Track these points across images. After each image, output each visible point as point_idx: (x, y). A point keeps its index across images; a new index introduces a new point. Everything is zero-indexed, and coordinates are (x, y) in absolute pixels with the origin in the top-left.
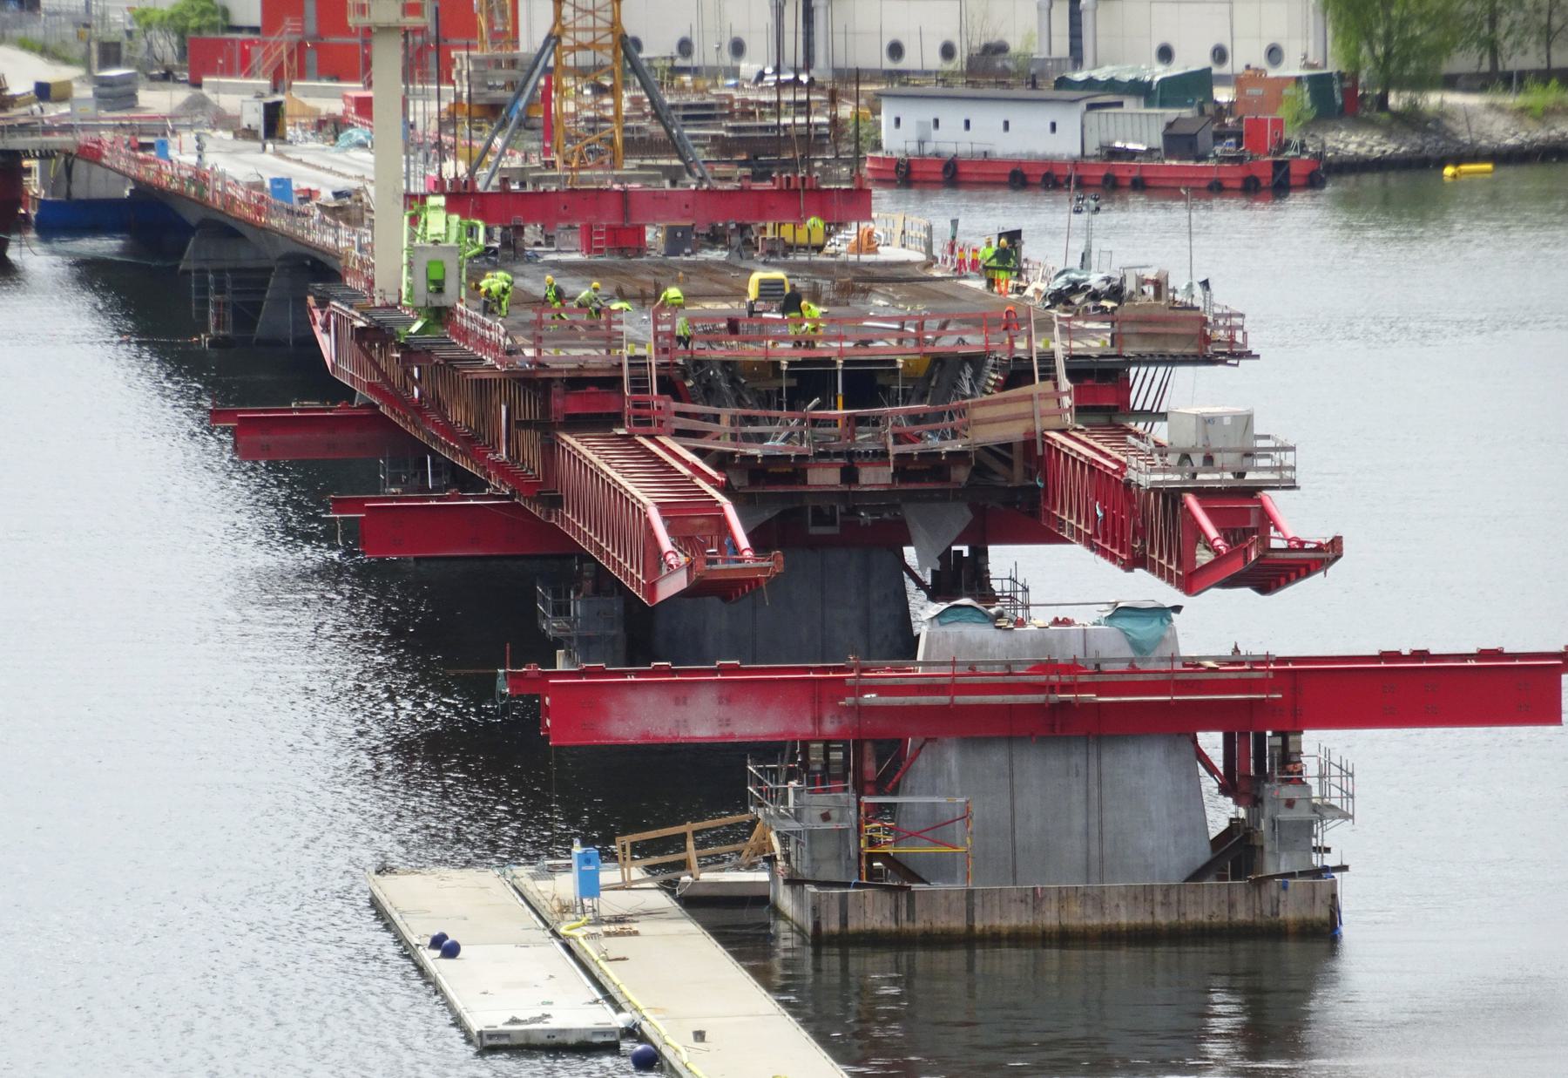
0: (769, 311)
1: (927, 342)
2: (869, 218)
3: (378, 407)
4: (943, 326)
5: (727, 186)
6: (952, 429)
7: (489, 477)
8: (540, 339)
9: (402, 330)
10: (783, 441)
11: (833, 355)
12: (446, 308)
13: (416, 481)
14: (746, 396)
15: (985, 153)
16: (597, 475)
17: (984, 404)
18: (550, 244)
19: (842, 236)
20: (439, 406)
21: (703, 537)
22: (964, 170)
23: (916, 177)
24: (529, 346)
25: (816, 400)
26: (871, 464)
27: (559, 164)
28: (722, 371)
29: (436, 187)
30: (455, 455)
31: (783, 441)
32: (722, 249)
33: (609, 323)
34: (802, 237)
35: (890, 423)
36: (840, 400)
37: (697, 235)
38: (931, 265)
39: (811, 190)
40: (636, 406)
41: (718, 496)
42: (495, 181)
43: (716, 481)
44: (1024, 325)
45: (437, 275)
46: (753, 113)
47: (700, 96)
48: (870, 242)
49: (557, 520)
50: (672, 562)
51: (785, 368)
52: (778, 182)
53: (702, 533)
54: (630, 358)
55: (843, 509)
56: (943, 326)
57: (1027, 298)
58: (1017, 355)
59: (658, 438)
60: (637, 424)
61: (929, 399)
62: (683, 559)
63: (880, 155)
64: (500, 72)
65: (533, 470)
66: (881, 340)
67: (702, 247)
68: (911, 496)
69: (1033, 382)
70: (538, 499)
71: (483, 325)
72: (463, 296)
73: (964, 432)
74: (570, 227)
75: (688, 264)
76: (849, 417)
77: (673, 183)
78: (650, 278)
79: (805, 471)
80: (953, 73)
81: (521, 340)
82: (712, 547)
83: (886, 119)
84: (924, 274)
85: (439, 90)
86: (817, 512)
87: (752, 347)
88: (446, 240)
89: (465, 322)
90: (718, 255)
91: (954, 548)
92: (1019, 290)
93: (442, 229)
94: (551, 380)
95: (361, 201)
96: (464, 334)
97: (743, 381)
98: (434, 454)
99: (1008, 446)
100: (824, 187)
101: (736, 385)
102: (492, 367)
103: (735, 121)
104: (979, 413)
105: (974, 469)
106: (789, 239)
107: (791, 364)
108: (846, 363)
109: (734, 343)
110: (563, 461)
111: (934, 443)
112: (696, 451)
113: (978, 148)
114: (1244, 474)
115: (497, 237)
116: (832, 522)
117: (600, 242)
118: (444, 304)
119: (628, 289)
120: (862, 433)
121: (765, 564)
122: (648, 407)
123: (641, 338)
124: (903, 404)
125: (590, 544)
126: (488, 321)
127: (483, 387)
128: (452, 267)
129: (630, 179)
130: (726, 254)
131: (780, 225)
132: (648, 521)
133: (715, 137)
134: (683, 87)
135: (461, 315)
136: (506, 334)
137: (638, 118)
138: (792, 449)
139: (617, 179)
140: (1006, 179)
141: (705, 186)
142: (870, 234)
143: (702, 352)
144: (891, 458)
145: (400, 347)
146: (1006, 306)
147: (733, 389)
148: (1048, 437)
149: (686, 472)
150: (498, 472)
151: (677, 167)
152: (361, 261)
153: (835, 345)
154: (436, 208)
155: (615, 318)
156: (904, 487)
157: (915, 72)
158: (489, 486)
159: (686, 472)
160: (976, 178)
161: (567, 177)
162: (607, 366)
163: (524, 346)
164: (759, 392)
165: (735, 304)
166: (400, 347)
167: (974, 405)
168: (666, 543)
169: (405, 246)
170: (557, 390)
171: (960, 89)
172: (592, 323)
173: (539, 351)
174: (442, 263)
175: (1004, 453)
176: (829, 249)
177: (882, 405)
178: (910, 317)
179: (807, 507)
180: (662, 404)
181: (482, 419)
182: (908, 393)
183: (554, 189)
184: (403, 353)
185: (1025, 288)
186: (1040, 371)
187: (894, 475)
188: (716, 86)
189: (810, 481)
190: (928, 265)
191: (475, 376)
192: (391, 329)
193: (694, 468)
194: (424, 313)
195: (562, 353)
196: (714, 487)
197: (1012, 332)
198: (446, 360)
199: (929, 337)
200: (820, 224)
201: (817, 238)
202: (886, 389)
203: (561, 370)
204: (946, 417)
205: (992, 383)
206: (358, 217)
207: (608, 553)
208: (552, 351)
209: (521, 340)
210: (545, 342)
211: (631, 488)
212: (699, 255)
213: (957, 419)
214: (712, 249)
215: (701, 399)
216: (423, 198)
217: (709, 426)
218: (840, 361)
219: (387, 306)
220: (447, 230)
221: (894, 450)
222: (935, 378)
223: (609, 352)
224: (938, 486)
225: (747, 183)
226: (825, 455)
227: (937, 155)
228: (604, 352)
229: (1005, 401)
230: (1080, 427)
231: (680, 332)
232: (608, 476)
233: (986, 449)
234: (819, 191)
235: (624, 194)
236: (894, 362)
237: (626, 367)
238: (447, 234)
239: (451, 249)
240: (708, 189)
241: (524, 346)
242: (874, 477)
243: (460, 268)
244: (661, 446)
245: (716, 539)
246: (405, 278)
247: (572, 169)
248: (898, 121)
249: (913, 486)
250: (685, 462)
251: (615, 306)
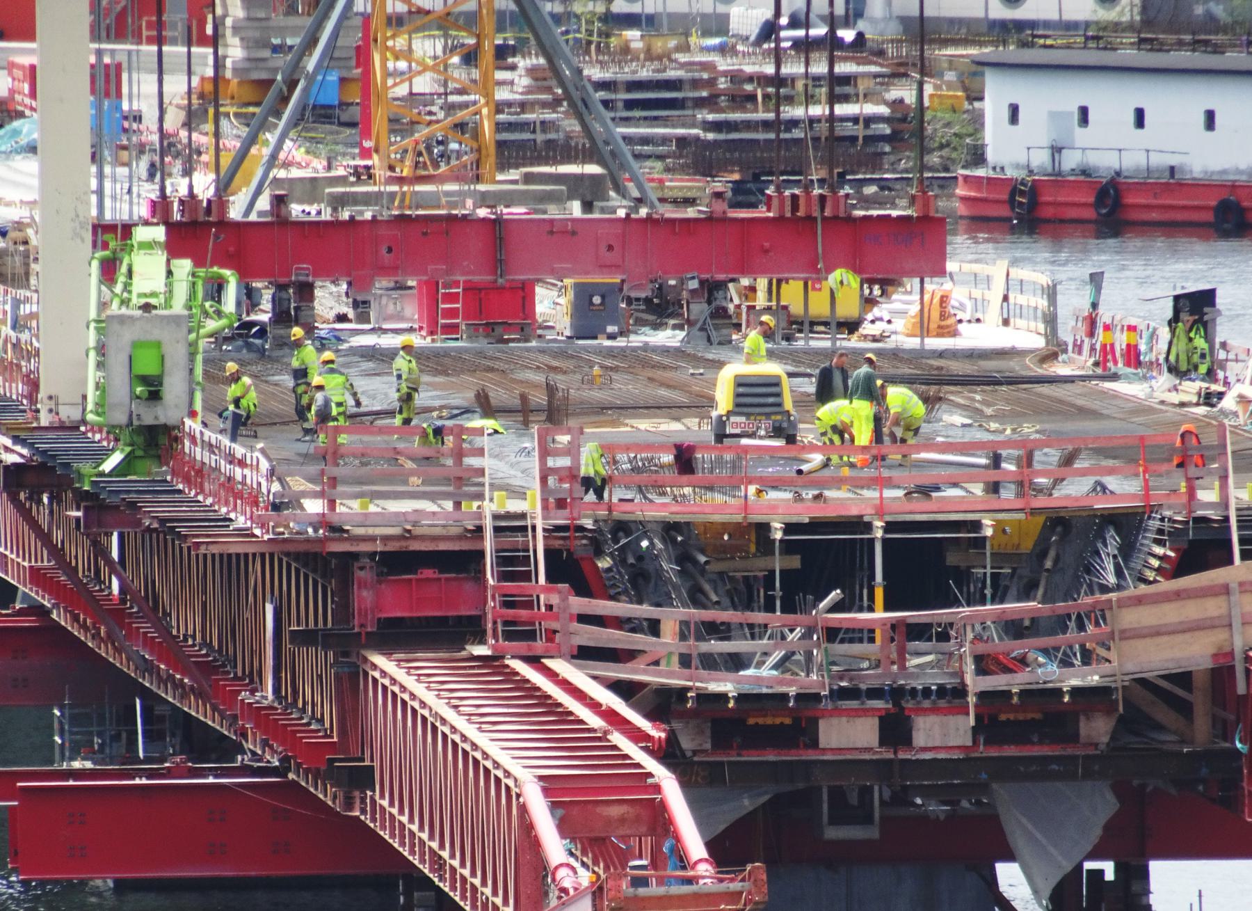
0: (752, 435)
1: (1039, 490)
2: (941, 272)
3: (49, 612)
4: (1068, 460)
5: (691, 213)
6: (1083, 647)
7: (244, 735)
8: (334, 481)
9: (86, 468)
10: (775, 667)
11: (868, 513)
12: (166, 429)
13: (120, 748)
14: (707, 587)
15: (1172, 169)
16: (434, 728)
17: (1139, 601)
18: (363, 318)
19: (897, 306)
20: (153, 607)
21: (624, 838)
22: (1130, 200)
23: (1048, 212)
24: (315, 495)
25: (835, 595)
26: (935, 710)
27: (380, 173)
28: (664, 541)
29: (154, 214)
30: (183, 697)
31: (775, 667)
32: (675, 327)
33: (459, 454)
34: (819, 306)
35: (970, 636)
36: (879, 594)
37: (629, 301)
38: (1054, 356)
39: (835, 218)
40: (508, 605)
42: (264, 203)
43: (648, 738)
44: (1213, 460)
45: (147, 366)
46: (752, 98)
47: (656, 64)
48: (943, 316)
49: (363, 811)
50: (567, 884)
51: (778, 535)
52: (775, 203)
53: (621, 832)
54: (496, 517)
55: (887, 794)
56: (1068, 460)
57: (1223, 412)
58: (1200, 513)
59: (547, 662)
60: (509, 636)
61: (1040, 592)
62: (585, 878)
63: (981, 172)
64: (293, 21)
65: (321, 721)
66: (955, 485)
67: (641, 322)
68: (1006, 770)
69: (1230, 561)
70: (328, 774)
71: (231, 458)
72: (198, 406)
73: (1102, 652)
74: (401, 287)
75: (610, 353)
76: (894, 626)
77: (588, 206)
78: (539, 378)
79: (814, 722)
80: (1116, 27)
81: (298, 484)
82: (640, 857)
83: (993, 107)
84: (1040, 371)
85: (189, 53)
86: (837, 795)
87: (719, 498)
88: (168, 304)
89: (199, 454)
90: (669, 337)
91: (1089, 865)
92: (1209, 399)
93: (159, 284)
94: (354, 556)
95: (26, 243)
96: (196, 475)
97: (703, 559)
98: (146, 694)
99: (1183, 679)
100: (859, 213)
101: (689, 566)
102: (246, 533)
103: (721, 111)
104: (1131, 618)
105: (1121, 720)
106: (797, 308)
107: (789, 528)
108: (890, 527)
109: (687, 490)
110: (376, 707)
111: (1047, 672)
112: (624, 689)
113: (1160, 160)
115: (266, 304)
116: (867, 820)
117: (452, 313)
118: (162, 420)
119: (499, 395)
120: (919, 654)
121: (736, 886)
122: (529, 605)
123: (518, 481)
124: (993, 602)
125: (422, 854)
126: (239, 450)
127: (233, 566)
128: (176, 353)
129: (509, 199)
130: (681, 335)
131: (779, 282)
132: (523, 809)
133: (682, 141)
134: (626, 50)
135: (193, 440)
136: (272, 473)
137: (544, 105)
138: (790, 683)
139: (484, 199)
140: (1209, 217)
141: (643, 212)
142: (944, 300)
143: (627, 507)
144: (972, 700)
145: (82, 498)
146: (1180, 423)
147: (683, 573)
149: (595, 721)
150: (257, 726)
151: (593, 177)
152: (17, 346)
153: (871, 494)
154: (149, 245)
155: (469, 441)
156: (993, 753)
157: (1047, 24)
158: (243, 752)
159: (595, 721)
160: (1155, 216)
161: (392, 195)
162: (454, 531)
163: (305, 494)
164: (732, 579)
165: (693, 422)
166: (82, 498)
167: (1122, 604)
168: (555, 847)
169: (93, 314)
170: (363, 574)
171: (1128, 55)
172: (427, 452)
173: (332, 504)
174: (158, 344)
175: (1180, 692)
176: (867, 329)
177: (956, 603)
178: (1008, 444)
179: (820, 788)
180: (555, 600)
181: (231, 630)
182: (1003, 583)
183: (368, 215)
184: (87, 510)
185: (1221, 395)
186: (1242, 541)
187: (976, 730)
188: (685, 48)
189: (823, 743)
190: (1050, 356)
191: (215, 550)
192: (67, 466)
193: (611, 716)
194: (125, 436)
195: (372, 508)
196: (646, 749)
197: (1192, 471)
198: (163, 521)
199: (1042, 480)
200: (853, 281)
201: (848, 307)
202: (963, 576)
203: (372, 539)
204: (1072, 624)
205: (1155, 563)
206: (20, 270)
207: (453, 869)
208: (356, 505)
209: (298, 484)
210: (340, 488)
211: (494, 750)
212: (633, 337)
213: (1090, 628)
214: (656, 326)
215: (626, 592)
216: (126, 230)
217: (640, 640)
218: (878, 524)
219: (62, 427)
220: (169, 286)
221: (974, 683)
222: (1052, 554)
223: (458, 505)
225: (720, 207)
226: (851, 693)
227: (1084, 172)
228: (449, 505)
229: (1178, 595)
231: (586, 470)
232: (454, 730)
233: (1143, 682)
234: (850, 219)
235: (496, 226)
236: (976, 526)
237: (489, 533)
238: (170, 292)
239: (176, 319)
240: (649, 219)
241: (305, 494)
243: (192, 356)
244: (551, 674)
245: (648, 842)
246: (92, 375)
247: (401, 180)
248: (1014, 111)
249: (1011, 751)
250: (594, 706)
251: (477, 423)
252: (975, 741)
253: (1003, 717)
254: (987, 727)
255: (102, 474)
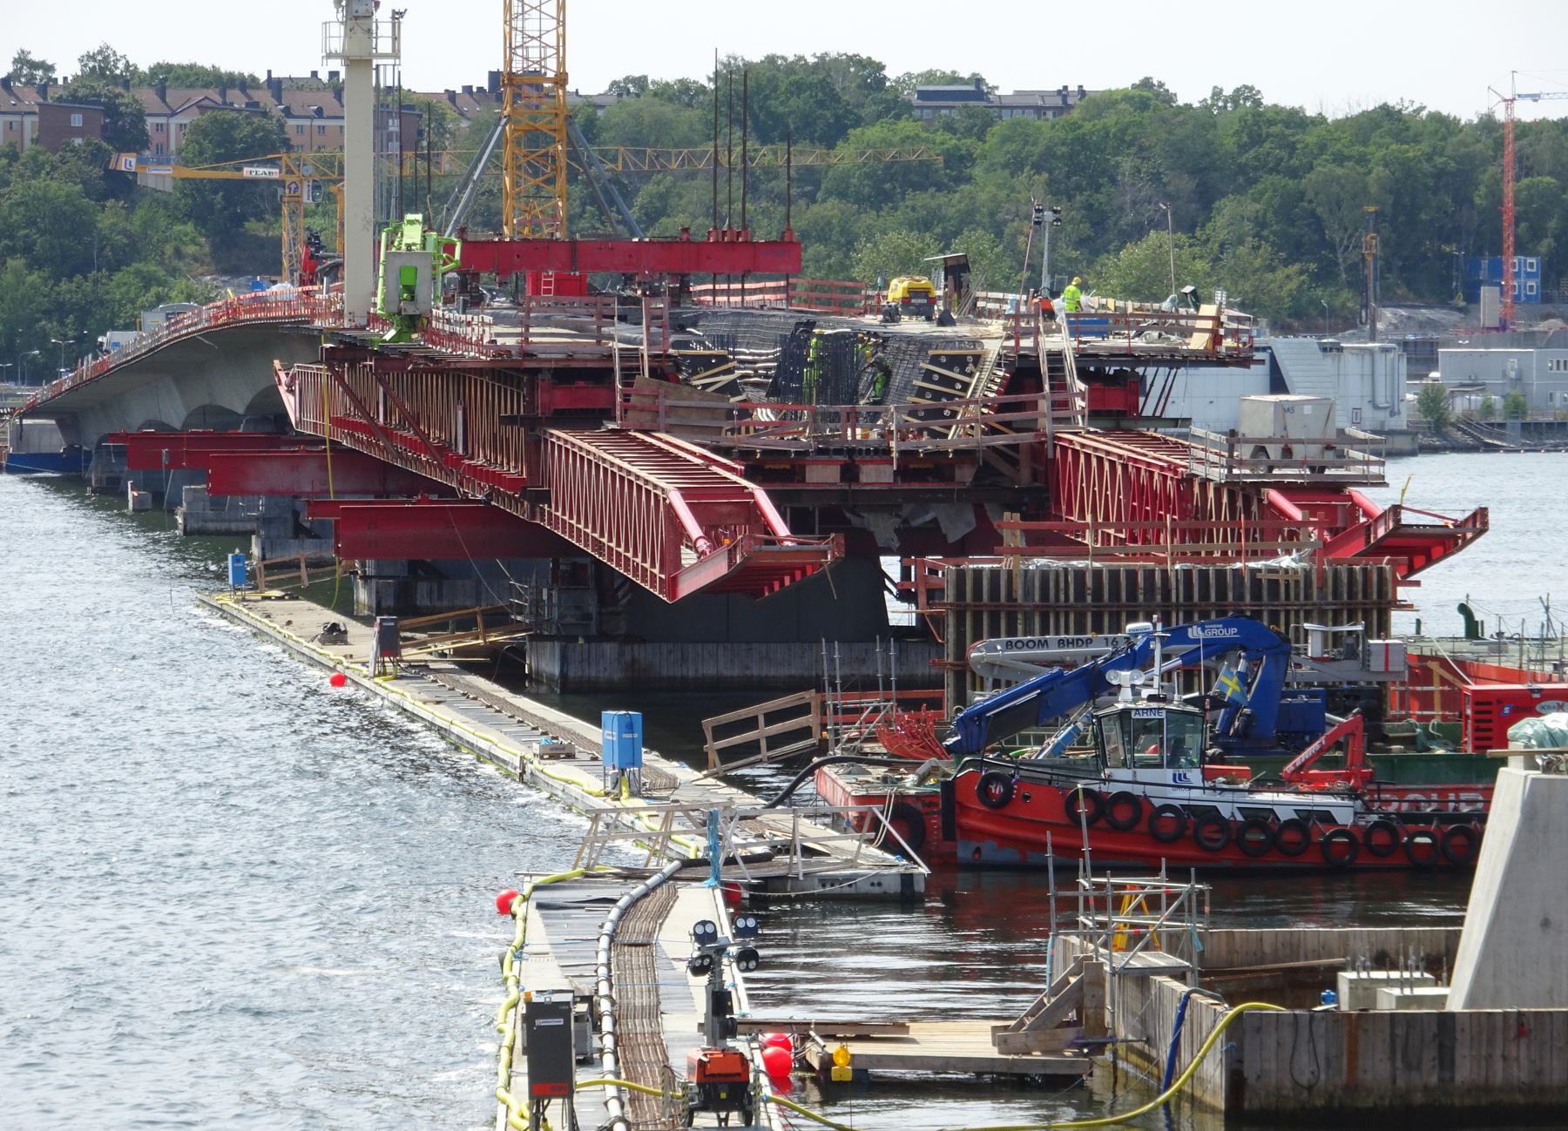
16: (597, 466)
26: (872, 462)
41: (744, 483)
93: (418, 240)
94: (537, 371)
114: (1322, 469)
125: (586, 541)
132: (670, 508)
144: (894, 455)
148: (1061, 439)
154: (411, 222)
187: (896, 473)
203: (550, 360)
224: (942, 486)
230: (1092, 429)
242: (875, 475)
249: (916, 486)
252: (895, 480)
253: (911, 466)
254: (903, 473)
255: (385, 341)
